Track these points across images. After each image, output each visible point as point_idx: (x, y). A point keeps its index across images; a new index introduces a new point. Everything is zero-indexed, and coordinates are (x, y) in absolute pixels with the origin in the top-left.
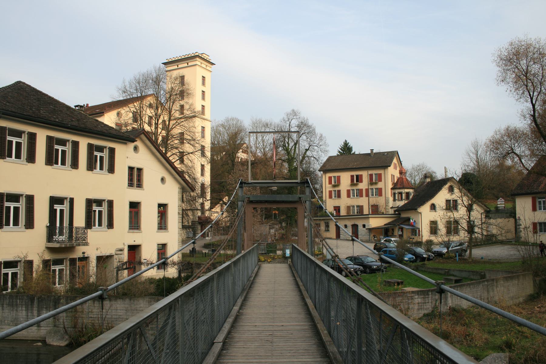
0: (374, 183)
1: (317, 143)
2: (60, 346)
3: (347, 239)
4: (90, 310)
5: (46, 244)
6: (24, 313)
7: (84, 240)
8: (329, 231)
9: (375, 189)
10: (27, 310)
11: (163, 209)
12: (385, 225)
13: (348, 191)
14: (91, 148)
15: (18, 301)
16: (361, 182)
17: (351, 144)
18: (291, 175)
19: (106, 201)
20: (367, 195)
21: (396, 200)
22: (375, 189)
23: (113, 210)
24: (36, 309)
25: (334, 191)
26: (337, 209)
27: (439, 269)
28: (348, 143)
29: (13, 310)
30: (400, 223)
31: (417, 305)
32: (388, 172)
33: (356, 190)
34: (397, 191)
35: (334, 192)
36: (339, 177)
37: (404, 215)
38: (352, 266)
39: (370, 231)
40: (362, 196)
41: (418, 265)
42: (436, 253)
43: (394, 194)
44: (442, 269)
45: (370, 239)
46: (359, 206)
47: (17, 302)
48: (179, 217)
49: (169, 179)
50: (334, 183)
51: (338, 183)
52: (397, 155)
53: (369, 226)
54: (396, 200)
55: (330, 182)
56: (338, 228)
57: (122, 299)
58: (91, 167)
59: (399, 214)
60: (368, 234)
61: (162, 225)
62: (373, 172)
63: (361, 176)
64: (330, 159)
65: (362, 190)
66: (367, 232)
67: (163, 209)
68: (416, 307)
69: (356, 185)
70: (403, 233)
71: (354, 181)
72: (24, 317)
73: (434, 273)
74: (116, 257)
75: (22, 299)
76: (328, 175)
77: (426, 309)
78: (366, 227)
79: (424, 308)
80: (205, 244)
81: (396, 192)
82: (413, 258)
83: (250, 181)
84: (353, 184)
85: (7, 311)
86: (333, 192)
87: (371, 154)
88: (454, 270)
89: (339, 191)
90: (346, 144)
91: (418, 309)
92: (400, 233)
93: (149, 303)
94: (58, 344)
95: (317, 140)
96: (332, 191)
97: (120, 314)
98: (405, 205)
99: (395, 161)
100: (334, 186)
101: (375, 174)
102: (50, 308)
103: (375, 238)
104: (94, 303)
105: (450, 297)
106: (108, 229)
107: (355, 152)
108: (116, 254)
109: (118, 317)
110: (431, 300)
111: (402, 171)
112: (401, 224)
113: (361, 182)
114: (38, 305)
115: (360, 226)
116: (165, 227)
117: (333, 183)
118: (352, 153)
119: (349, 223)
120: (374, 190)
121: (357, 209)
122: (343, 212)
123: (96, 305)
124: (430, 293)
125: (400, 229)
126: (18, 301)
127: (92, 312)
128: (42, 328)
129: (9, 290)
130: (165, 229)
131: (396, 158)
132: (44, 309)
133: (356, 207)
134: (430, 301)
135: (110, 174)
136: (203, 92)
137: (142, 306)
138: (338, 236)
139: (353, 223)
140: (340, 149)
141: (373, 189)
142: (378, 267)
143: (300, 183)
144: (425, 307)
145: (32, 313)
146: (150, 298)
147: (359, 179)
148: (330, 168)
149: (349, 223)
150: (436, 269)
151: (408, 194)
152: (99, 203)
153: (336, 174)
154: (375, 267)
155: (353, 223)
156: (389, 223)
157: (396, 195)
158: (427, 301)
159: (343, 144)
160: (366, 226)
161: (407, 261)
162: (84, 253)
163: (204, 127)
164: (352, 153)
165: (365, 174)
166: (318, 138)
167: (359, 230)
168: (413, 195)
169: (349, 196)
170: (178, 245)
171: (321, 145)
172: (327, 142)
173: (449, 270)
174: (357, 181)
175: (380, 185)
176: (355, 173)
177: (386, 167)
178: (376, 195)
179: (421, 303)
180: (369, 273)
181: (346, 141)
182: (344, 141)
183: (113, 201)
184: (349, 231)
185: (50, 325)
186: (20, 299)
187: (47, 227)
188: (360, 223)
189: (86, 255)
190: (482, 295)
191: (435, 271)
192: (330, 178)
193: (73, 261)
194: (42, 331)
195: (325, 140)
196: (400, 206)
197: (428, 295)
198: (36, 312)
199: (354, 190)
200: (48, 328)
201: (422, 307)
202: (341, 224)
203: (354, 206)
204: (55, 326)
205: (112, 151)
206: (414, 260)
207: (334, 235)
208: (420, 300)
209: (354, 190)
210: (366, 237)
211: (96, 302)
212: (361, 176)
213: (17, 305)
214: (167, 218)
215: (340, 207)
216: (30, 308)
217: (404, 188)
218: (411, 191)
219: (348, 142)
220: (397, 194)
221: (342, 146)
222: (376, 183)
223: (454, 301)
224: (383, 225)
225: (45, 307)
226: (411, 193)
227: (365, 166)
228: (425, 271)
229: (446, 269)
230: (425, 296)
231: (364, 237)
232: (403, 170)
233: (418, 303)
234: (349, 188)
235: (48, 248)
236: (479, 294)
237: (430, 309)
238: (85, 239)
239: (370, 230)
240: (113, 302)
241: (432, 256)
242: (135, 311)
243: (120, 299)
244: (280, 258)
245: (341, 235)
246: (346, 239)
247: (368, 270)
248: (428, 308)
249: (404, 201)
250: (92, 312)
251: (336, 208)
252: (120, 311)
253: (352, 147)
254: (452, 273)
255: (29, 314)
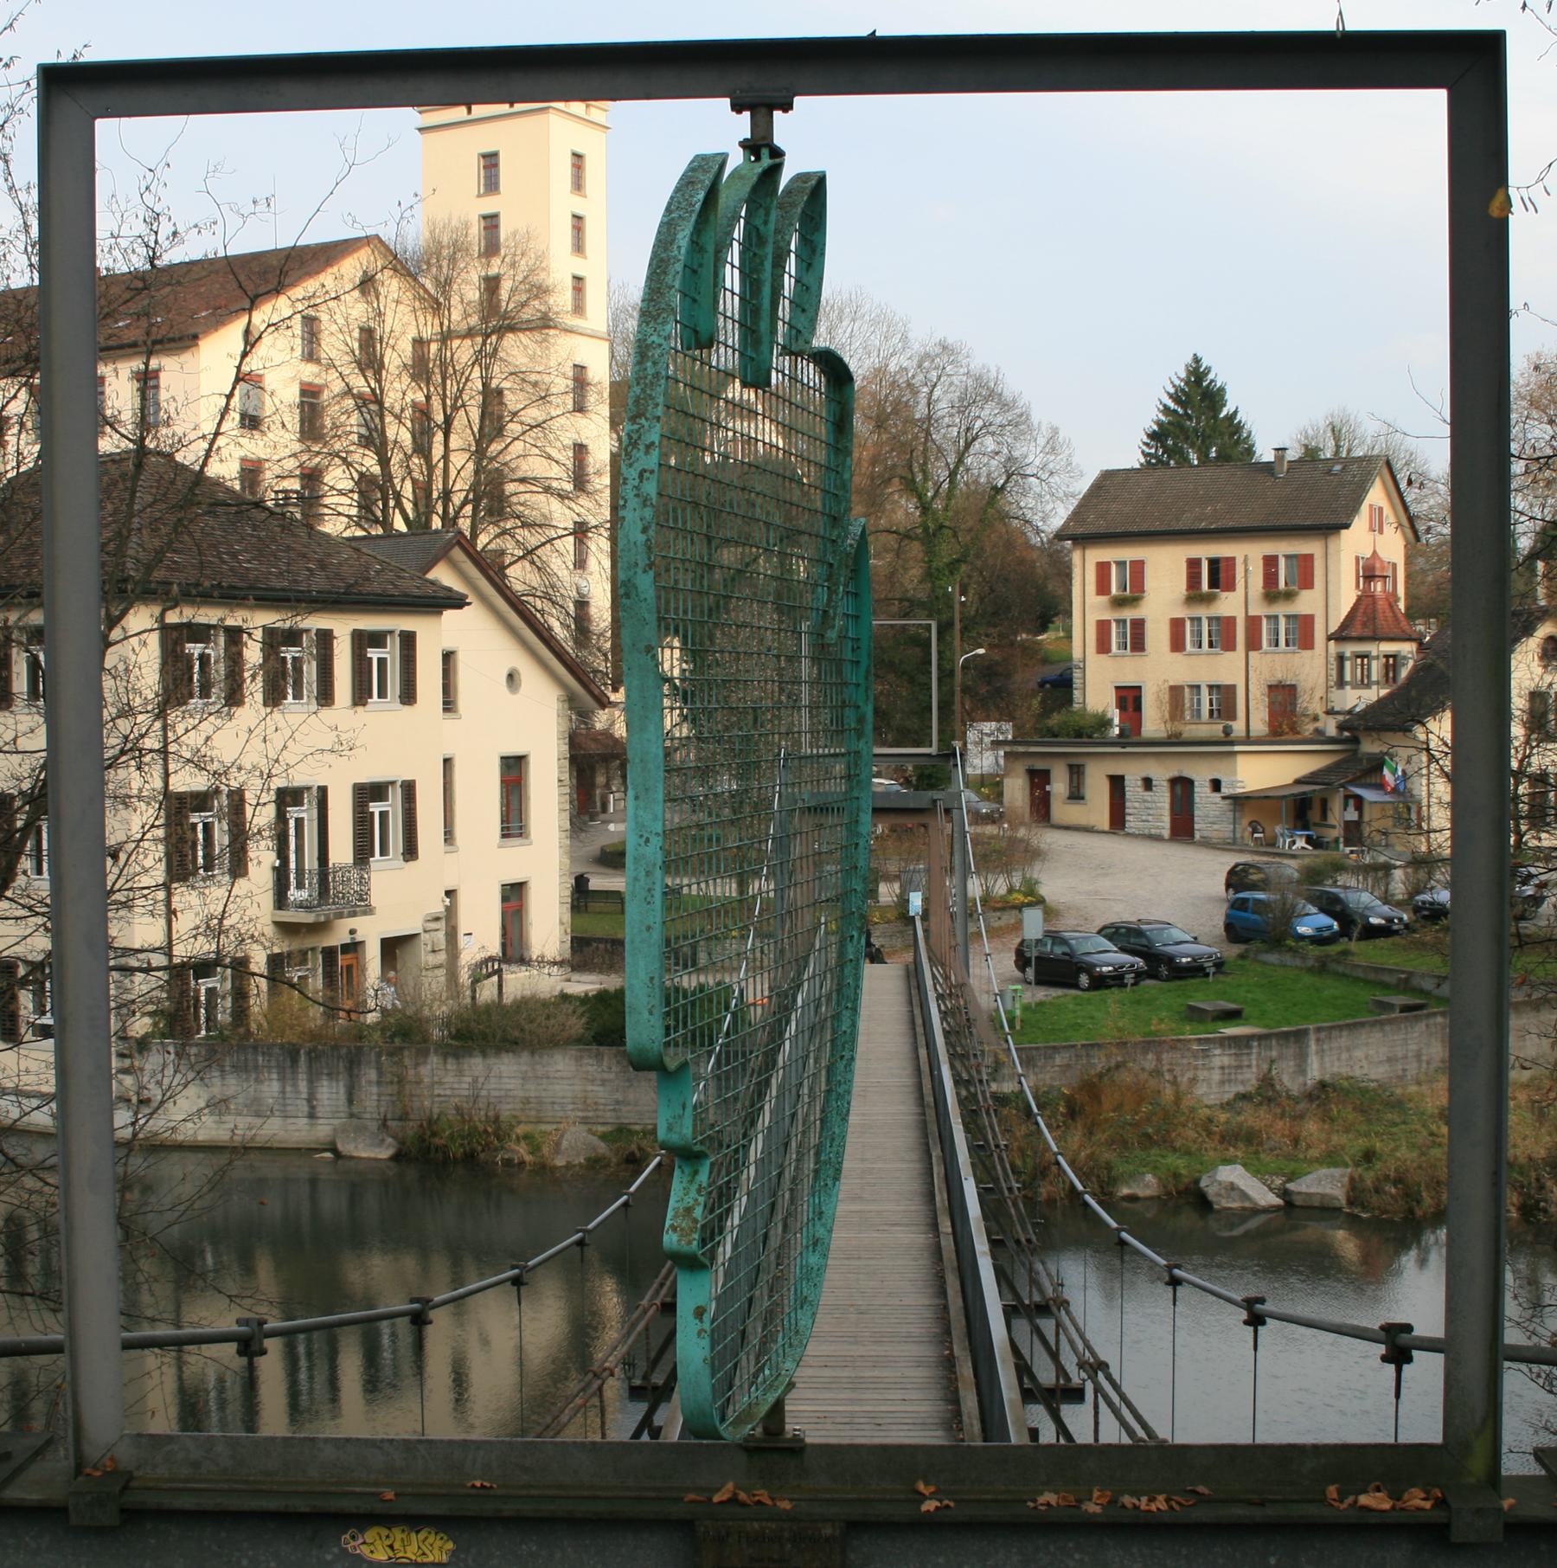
0: (1279, 593)
1: (1037, 462)
2: (376, 1160)
3: (1153, 831)
4: (436, 1079)
5: (273, 915)
6: (275, 1086)
7: (362, 900)
8: (1083, 798)
9: (1288, 617)
10: (282, 1079)
11: (514, 769)
12: (1298, 782)
13: (1177, 625)
14: (362, 641)
15: (260, 1058)
16: (1231, 587)
17: (1220, 374)
18: (933, 591)
19: (399, 783)
20: (1253, 644)
21: (1347, 683)
22: (1288, 617)
23: (415, 809)
24: (305, 1076)
25: (1118, 621)
26: (1130, 698)
27: (1384, 970)
28: (1208, 369)
29: (247, 1080)
30: (1350, 777)
31: (1217, 1071)
32: (1339, 551)
33: (1210, 619)
34: (1349, 649)
35: (1118, 627)
36: (1138, 567)
37: (1370, 747)
38: (1111, 958)
39: (1235, 804)
40: (1230, 646)
41: (1327, 956)
42: (1426, 909)
43: (1341, 659)
44: (1391, 971)
45: (1238, 835)
46: (1218, 687)
47: (257, 1060)
48: (560, 795)
49: (532, 677)
50: (1118, 589)
51: (1132, 595)
52: (1385, 471)
53: (1233, 784)
54: (1347, 683)
55: (1103, 588)
56: (1117, 783)
57: (513, 1052)
58: (361, 695)
59: (1355, 740)
60: (1230, 815)
61: (513, 823)
62: (1282, 548)
63: (1231, 561)
64: (1108, 482)
65: (1230, 622)
66: (1226, 808)
67: (514, 769)
68: (1216, 1076)
69: (1209, 599)
70: (1361, 816)
71: (1199, 583)
72: (276, 1095)
73: (1357, 979)
74: (425, 937)
75: (270, 1055)
76: (1096, 555)
77: (1243, 1082)
78: (1225, 791)
79: (1236, 1080)
80: (603, 850)
81: (1348, 654)
82: (1330, 927)
83: (806, 750)
84: (1194, 596)
85: (233, 1081)
86: (1114, 625)
87: (1277, 468)
88: (1423, 976)
89: (1139, 626)
90: (1197, 373)
91: (1222, 1082)
92: (1352, 815)
93: (577, 1060)
94: (372, 1155)
95: (1039, 449)
96: (1109, 622)
97: (508, 1087)
98: (1381, 702)
99: (1376, 495)
100: (1119, 603)
101: (1287, 557)
102: (338, 1073)
103: (1255, 831)
104: (445, 1063)
105: (1317, 1053)
106: (406, 860)
107: (1236, 412)
108: (425, 931)
109: (503, 1093)
110: (1257, 1060)
111: (1373, 568)
112: (1353, 782)
113: (1231, 587)
114: (310, 1067)
115: (1202, 786)
116: (521, 828)
117: (1114, 590)
118: (1222, 416)
119: (1161, 773)
120: (1282, 622)
121: (1211, 700)
122: (1153, 723)
123: (449, 1067)
124: (1255, 1044)
125: (1351, 802)
126: (260, 1058)
127: (440, 1083)
128: (321, 1121)
129: (203, 1032)
130: (520, 835)
131: (1384, 483)
132: (325, 1077)
133: (1205, 692)
134: (1254, 1062)
135: (407, 708)
136: (578, 218)
137: (560, 1067)
138: (1118, 819)
139: (1174, 772)
140: (1171, 396)
141: (1276, 617)
142: (1194, 960)
143: (938, 755)
144: (1240, 1077)
145: (295, 1085)
146: (580, 1050)
147: (1221, 574)
148: (1101, 526)
149: (1161, 773)
150: (1377, 970)
151: (1391, 664)
152: (376, 791)
153: (1128, 553)
154: (1184, 960)
155: (1176, 774)
156: (1314, 774)
157: (1348, 664)
158: (1246, 1063)
159: (1183, 375)
160: (1223, 784)
161: (1302, 937)
162: (352, 932)
163: (583, 367)
164: (1222, 416)
165: (1247, 556)
166: (1041, 441)
167: (1197, 799)
168: (1415, 666)
169: (1177, 644)
170: (561, 883)
171: (1052, 473)
172: (1075, 461)
173: (1411, 974)
174: (1214, 583)
175: (1307, 602)
176: (1205, 551)
177: (1331, 528)
178: (1287, 645)
179: (1229, 1067)
180: (1168, 979)
181: (1197, 360)
182: (1189, 359)
183: (414, 781)
184: (1162, 798)
185: (342, 1115)
186: (263, 1054)
187: (274, 868)
188: (1200, 774)
189: (359, 938)
190: (1424, 1051)
191: (1372, 976)
192: (1103, 569)
193: (329, 954)
194: (320, 1127)
195: (1070, 455)
196: (1358, 709)
197: (1250, 1047)
198: (305, 1083)
199: (1199, 619)
200: (336, 1122)
201: (1233, 1077)
202: (1133, 774)
203: (1198, 687)
204: (352, 1116)
205: (408, 640)
206: (1336, 933)
207: (1102, 819)
208: (1226, 1061)
209: (1199, 619)
210: (1223, 829)
211: (450, 1060)
212: (1231, 561)
213: (256, 1067)
214: (528, 798)
215: (1140, 688)
216: (289, 1075)
217: (1376, 638)
218: (1407, 648)
219: (1205, 363)
220: (1348, 659)
221: (1177, 382)
222: (1289, 596)
223: (1328, 1065)
224: (1290, 781)
225: (325, 1071)
226: (1405, 658)
227: (1245, 523)
228: (1344, 975)
229: (1403, 972)
230: (1240, 1049)
231: (1215, 827)
232: (1378, 565)
233: (1222, 1068)
234: (1180, 613)
235: (277, 924)
236: (1414, 1047)
237: (1254, 1082)
238: (363, 896)
239: (1240, 802)
240: (492, 1061)
241: (1401, 919)
242: (545, 1081)
243: (507, 1052)
244: (888, 922)
245: (1128, 818)
246: (1146, 832)
247: (1164, 970)
248: (1249, 1080)
249: (1375, 687)
250: (440, 1083)
251: (1124, 693)
252: (507, 1080)
253: (1222, 390)
254: (1415, 982)
255: (288, 1089)
